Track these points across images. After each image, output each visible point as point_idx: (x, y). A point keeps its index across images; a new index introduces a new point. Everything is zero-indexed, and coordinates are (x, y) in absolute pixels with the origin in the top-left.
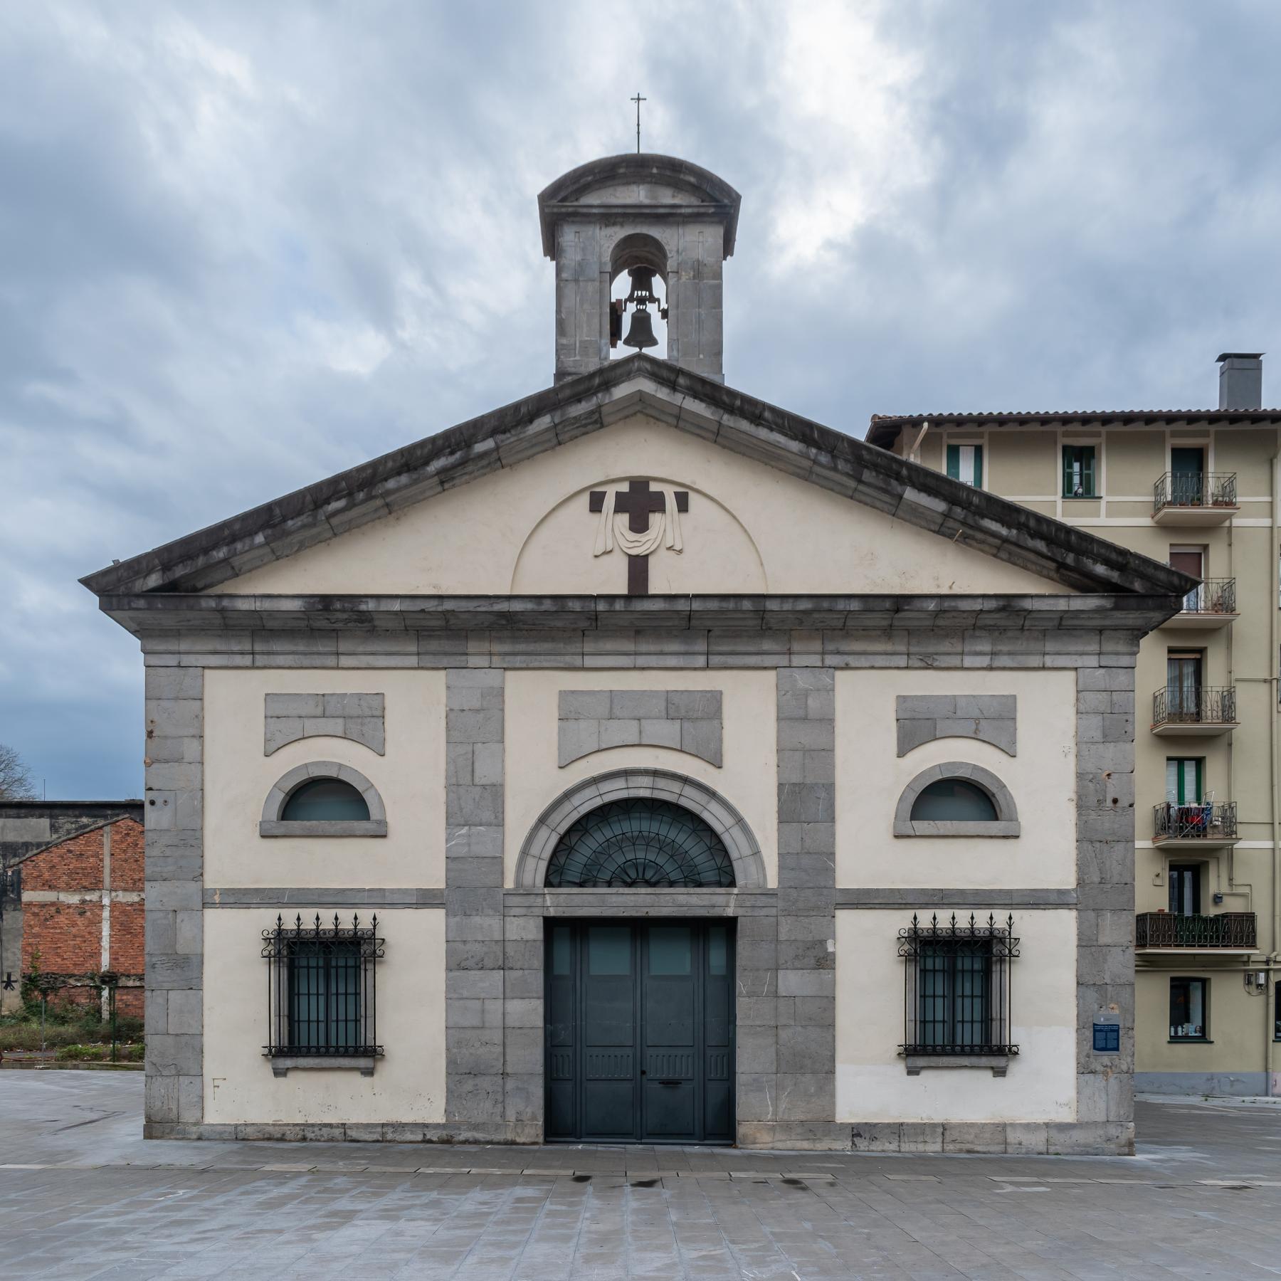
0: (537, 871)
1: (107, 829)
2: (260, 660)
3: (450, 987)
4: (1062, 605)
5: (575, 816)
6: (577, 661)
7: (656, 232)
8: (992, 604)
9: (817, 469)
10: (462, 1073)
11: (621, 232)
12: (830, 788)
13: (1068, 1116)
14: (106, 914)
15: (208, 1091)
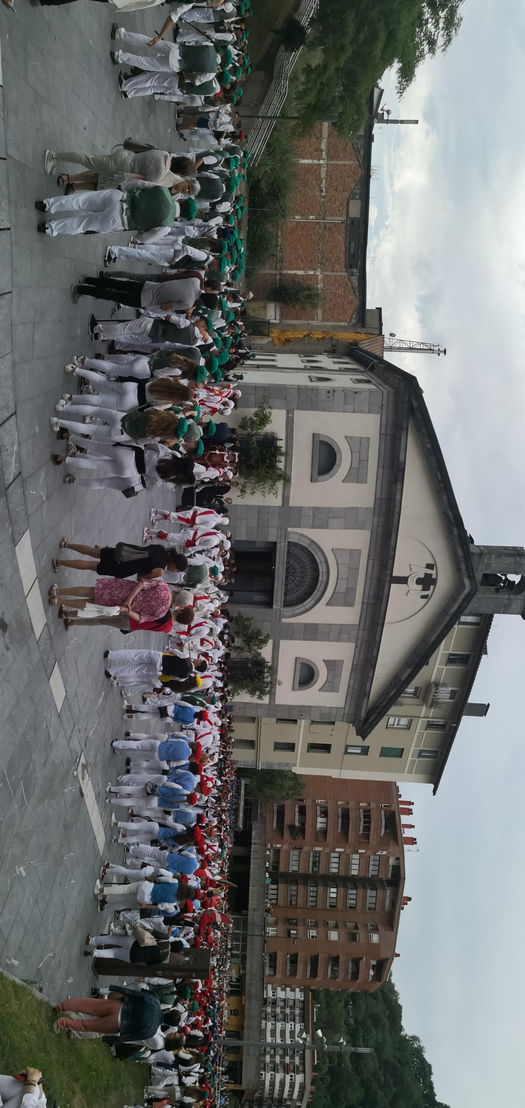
0: (293, 539)
1: (357, 163)
4: (364, 708)
5: (314, 553)
6: (372, 558)
8: (367, 691)
12: (315, 639)
14: (315, 162)
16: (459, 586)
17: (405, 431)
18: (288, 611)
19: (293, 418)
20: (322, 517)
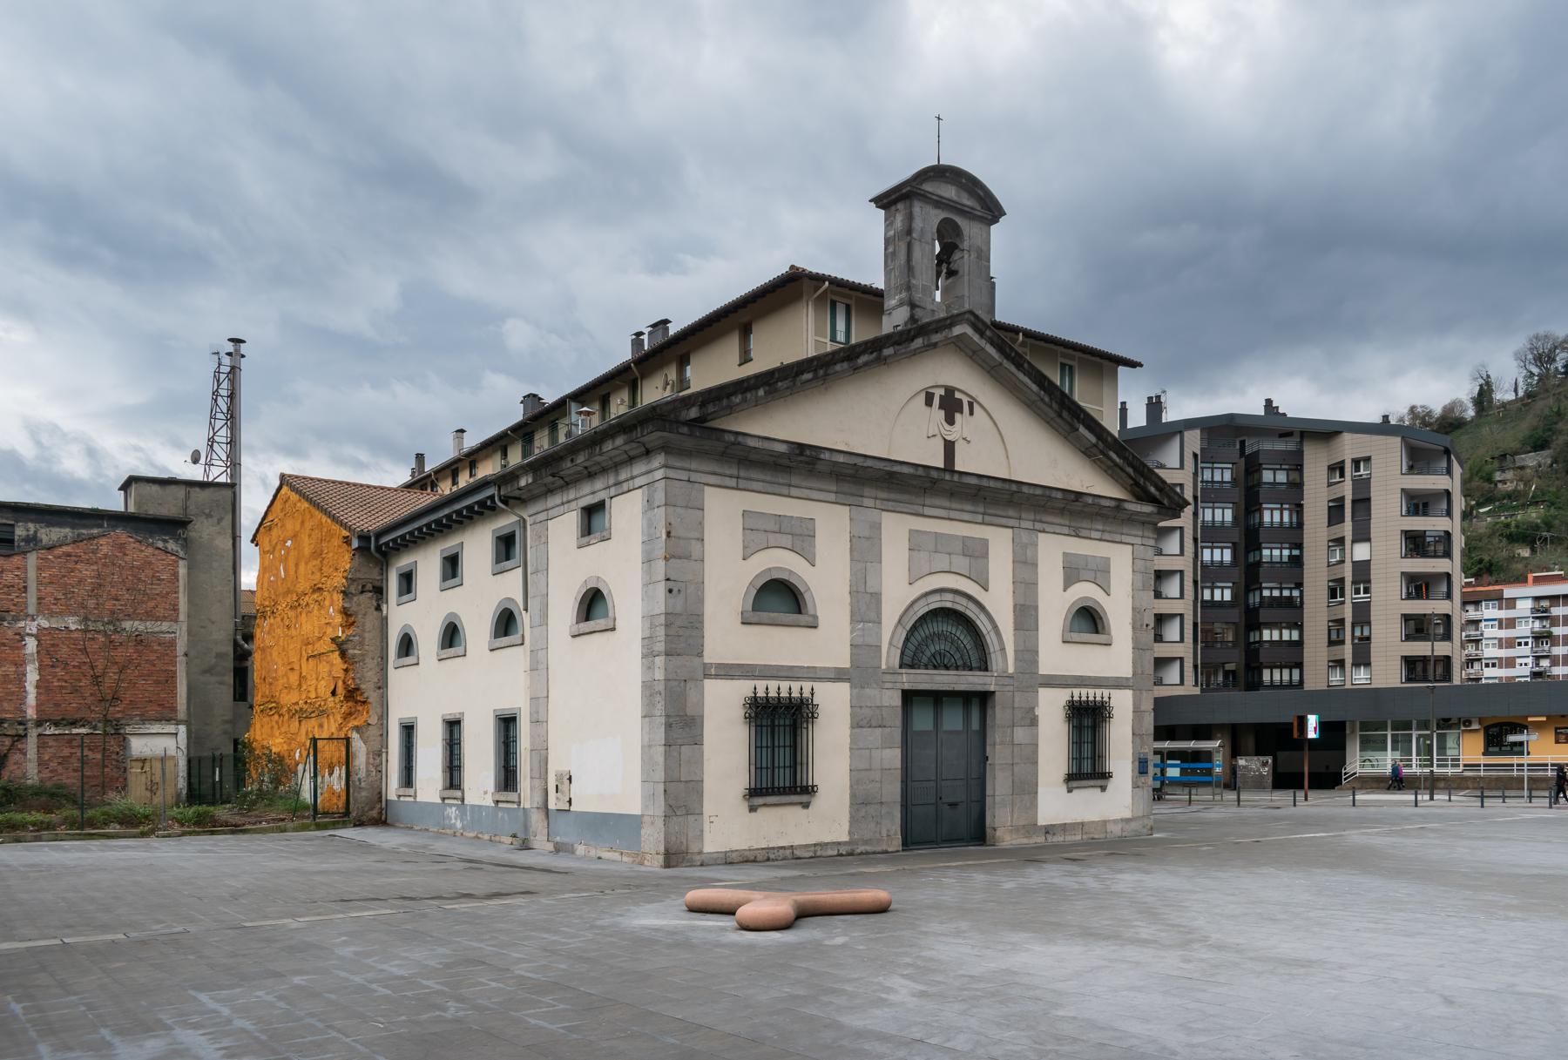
2: (742, 484)
3: (854, 739)
7: (959, 220)
9: (1040, 404)
10: (860, 803)
11: (943, 215)
12: (1036, 608)
13: (1128, 814)
15: (706, 827)
16: (960, 345)
17: (740, 439)
18: (995, 661)
19: (719, 666)
20: (865, 604)
